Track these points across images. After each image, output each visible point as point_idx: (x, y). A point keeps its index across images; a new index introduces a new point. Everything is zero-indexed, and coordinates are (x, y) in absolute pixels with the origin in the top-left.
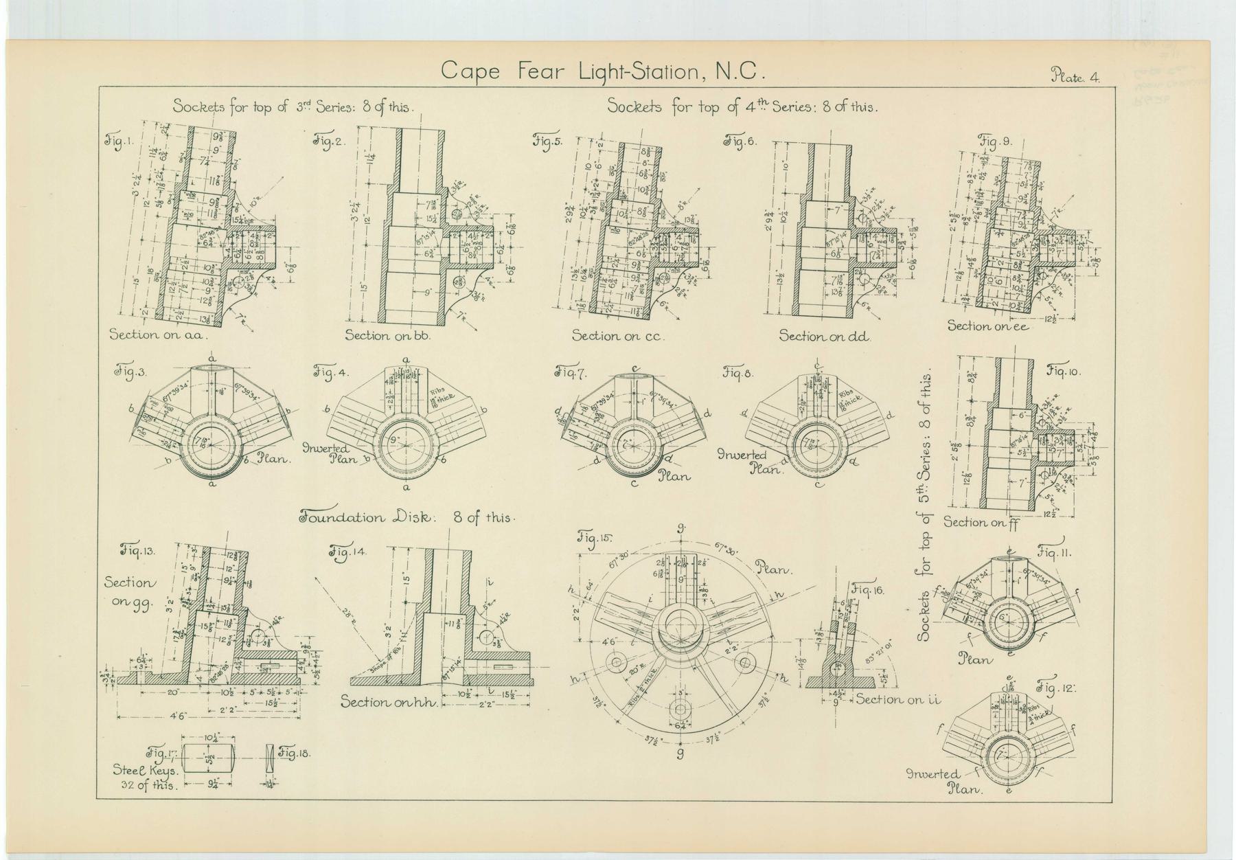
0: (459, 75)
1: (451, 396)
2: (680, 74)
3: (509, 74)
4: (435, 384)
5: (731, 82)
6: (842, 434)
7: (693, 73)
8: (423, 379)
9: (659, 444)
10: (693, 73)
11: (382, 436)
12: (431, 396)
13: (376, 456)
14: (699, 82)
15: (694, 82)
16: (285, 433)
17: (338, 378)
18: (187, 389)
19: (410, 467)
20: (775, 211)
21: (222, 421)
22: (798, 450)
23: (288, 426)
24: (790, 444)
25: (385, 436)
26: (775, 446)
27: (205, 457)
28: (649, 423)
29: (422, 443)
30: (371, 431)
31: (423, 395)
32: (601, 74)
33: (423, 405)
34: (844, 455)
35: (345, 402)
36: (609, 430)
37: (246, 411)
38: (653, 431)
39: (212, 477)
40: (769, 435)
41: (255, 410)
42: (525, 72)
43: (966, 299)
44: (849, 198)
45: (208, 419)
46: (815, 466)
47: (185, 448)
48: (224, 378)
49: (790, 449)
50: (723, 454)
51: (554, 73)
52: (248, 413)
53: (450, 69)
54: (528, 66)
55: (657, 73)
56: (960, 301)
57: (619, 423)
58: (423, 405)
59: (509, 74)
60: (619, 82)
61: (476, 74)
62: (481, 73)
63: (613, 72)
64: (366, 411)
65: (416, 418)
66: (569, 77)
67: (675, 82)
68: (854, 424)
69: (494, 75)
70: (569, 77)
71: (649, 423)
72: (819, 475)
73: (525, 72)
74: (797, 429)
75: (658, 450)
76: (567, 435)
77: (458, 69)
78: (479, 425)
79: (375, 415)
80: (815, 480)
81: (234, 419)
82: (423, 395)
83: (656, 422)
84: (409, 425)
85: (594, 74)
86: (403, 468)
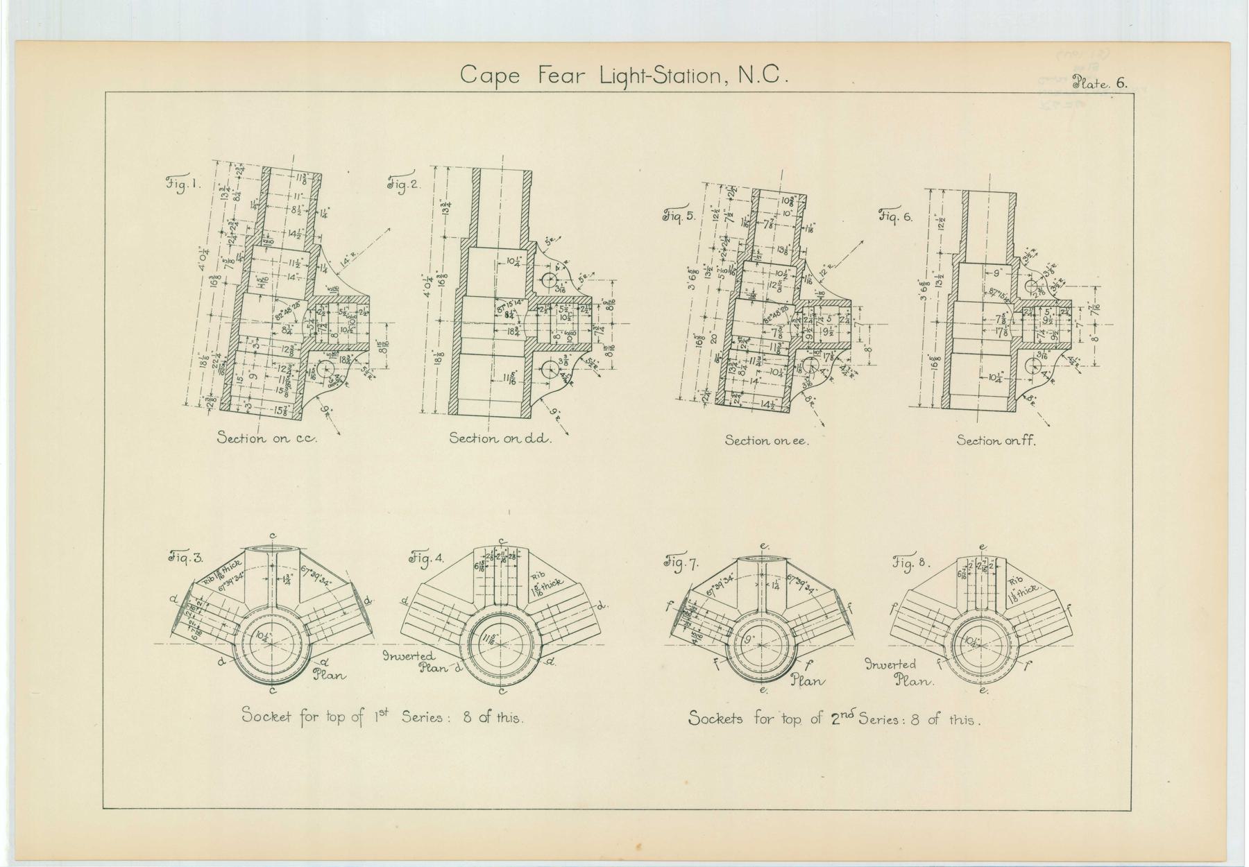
0: (479, 79)
1: (1033, 588)
2: (702, 78)
3: (529, 80)
4: (536, 567)
5: (754, 86)
6: (1010, 630)
7: (716, 76)
8: (522, 562)
9: (792, 643)
10: (716, 76)
11: (955, 635)
12: (533, 583)
13: (467, 660)
14: (722, 87)
15: (716, 86)
16: (364, 629)
17: (917, 568)
18: (732, 583)
19: (505, 671)
20: (434, 275)
21: (774, 618)
22: (475, 649)
23: (368, 623)
24: (948, 642)
25: (474, 634)
26: (443, 644)
27: (262, 656)
28: (780, 616)
29: (519, 641)
30: (941, 629)
31: (523, 580)
32: (622, 78)
33: (523, 593)
34: (1013, 656)
35: (911, 595)
36: (731, 624)
37: (800, 604)
38: (785, 627)
39: (272, 684)
40: (918, 631)
41: (813, 605)
42: (545, 77)
43: (211, 399)
44: (531, 248)
45: (268, 611)
46: (978, 670)
47: (732, 649)
48: (288, 561)
49: (948, 649)
50: (388, 656)
51: (574, 77)
52: (802, 610)
53: (469, 74)
54: (548, 71)
55: (702, 78)
56: (204, 403)
57: (742, 616)
58: (523, 593)
59: (529, 80)
60: (641, 87)
61: (495, 78)
62: (501, 77)
63: (635, 76)
64: (450, 601)
65: (993, 615)
66: (590, 81)
67: (697, 86)
68: (804, 619)
69: (513, 79)
70: (590, 81)
71: (780, 616)
72: (981, 680)
73: (545, 77)
74: (958, 623)
75: (791, 650)
76: (182, 628)
77: (478, 74)
78: (592, 620)
79: (460, 606)
80: (759, 686)
81: (300, 612)
82: (523, 580)
83: (789, 615)
84: (505, 620)
85: (616, 78)
86: (496, 671)
